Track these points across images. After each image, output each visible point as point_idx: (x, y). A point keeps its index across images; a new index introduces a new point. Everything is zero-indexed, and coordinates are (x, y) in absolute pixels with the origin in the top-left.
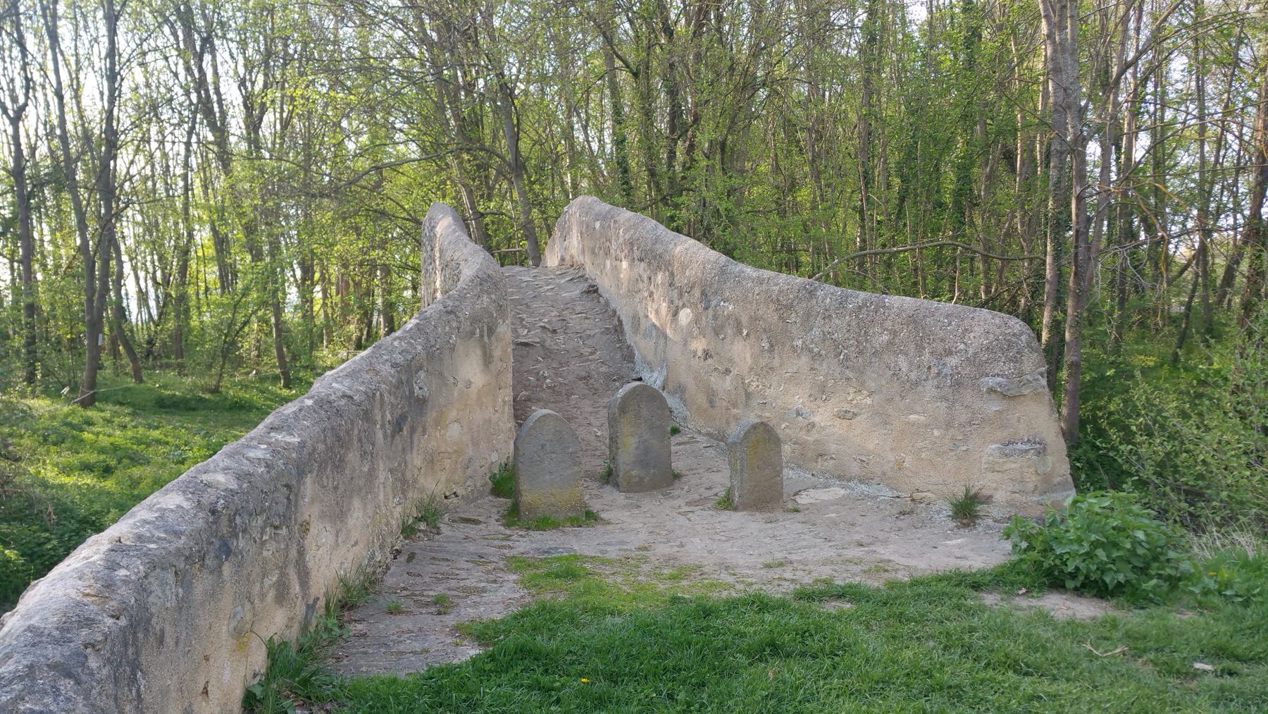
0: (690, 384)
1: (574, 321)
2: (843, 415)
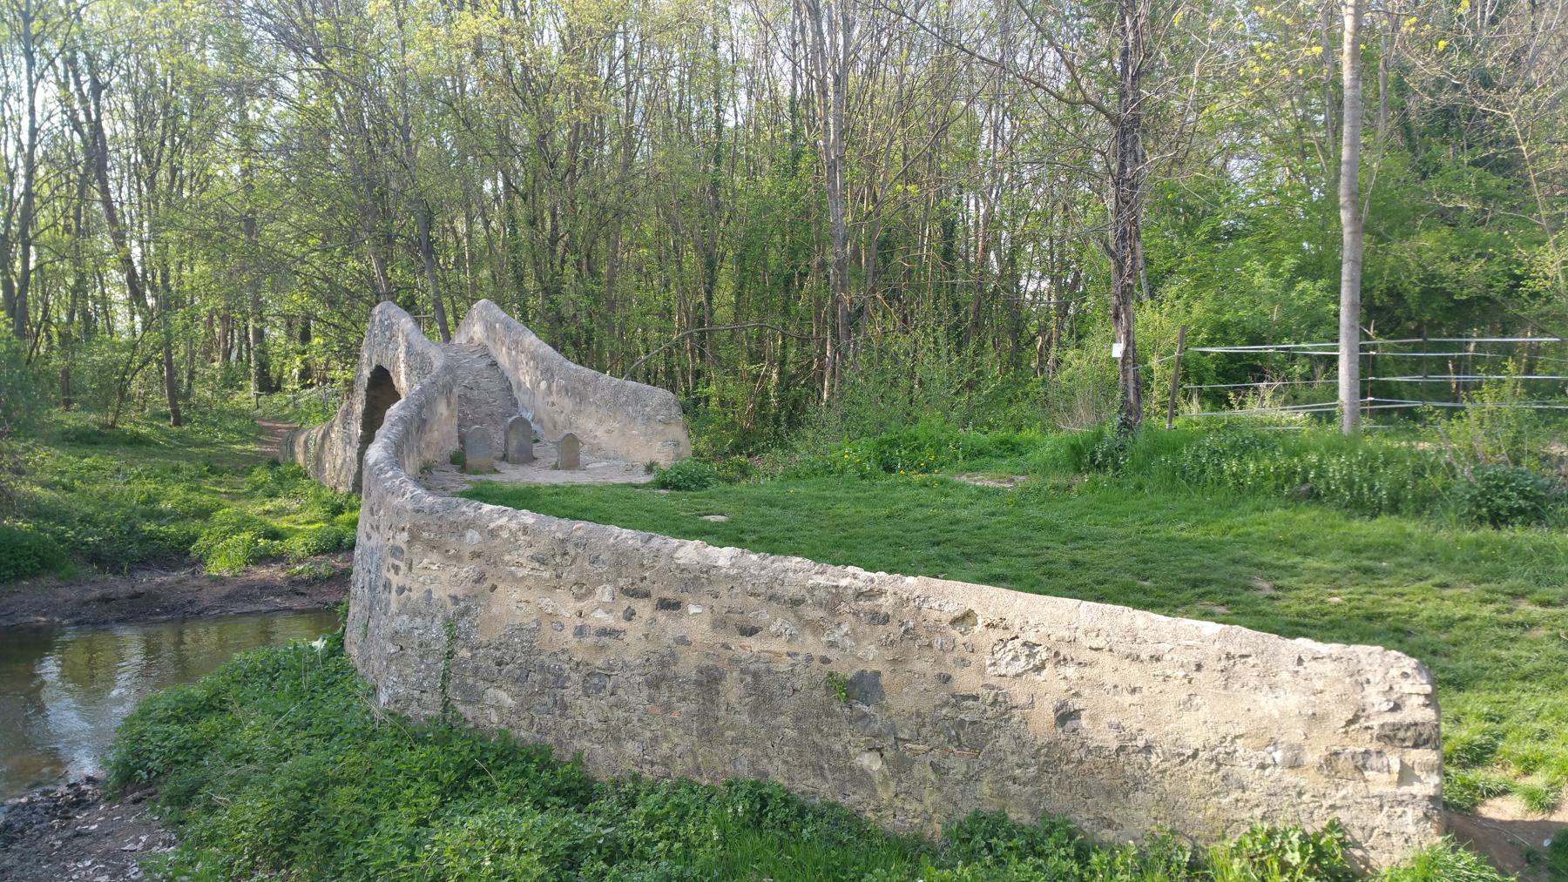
0: (546, 418)
1: (484, 383)
2: (608, 432)
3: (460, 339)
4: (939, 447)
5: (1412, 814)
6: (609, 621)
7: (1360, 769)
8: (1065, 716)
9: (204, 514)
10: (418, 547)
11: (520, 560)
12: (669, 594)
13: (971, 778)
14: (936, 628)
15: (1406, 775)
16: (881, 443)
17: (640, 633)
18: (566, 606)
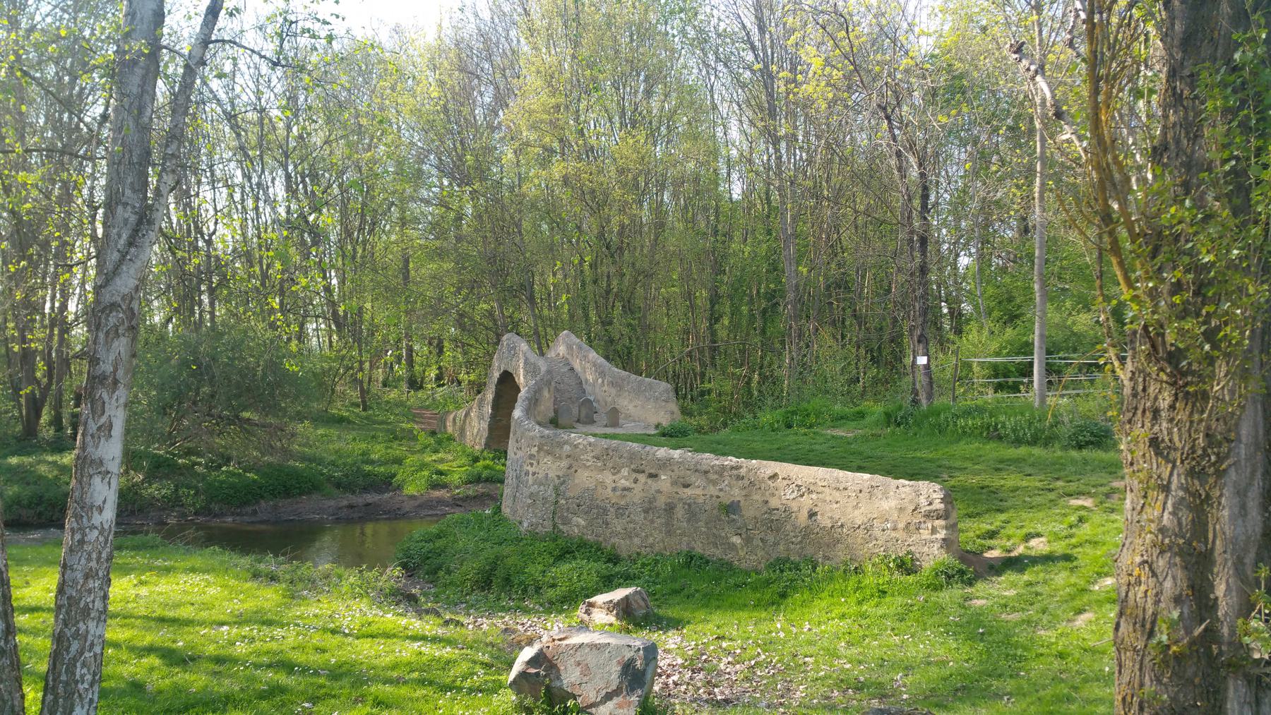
3: (551, 354)
4: (818, 414)
5: (937, 545)
6: (626, 484)
7: (918, 529)
8: (812, 515)
9: (398, 461)
10: (542, 454)
11: (588, 457)
12: (652, 471)
13: (776, 544)
14: (763, 481)
15: (934, 531)
16: (787, 412)
17: (640, 488)
18: (608, 478)
